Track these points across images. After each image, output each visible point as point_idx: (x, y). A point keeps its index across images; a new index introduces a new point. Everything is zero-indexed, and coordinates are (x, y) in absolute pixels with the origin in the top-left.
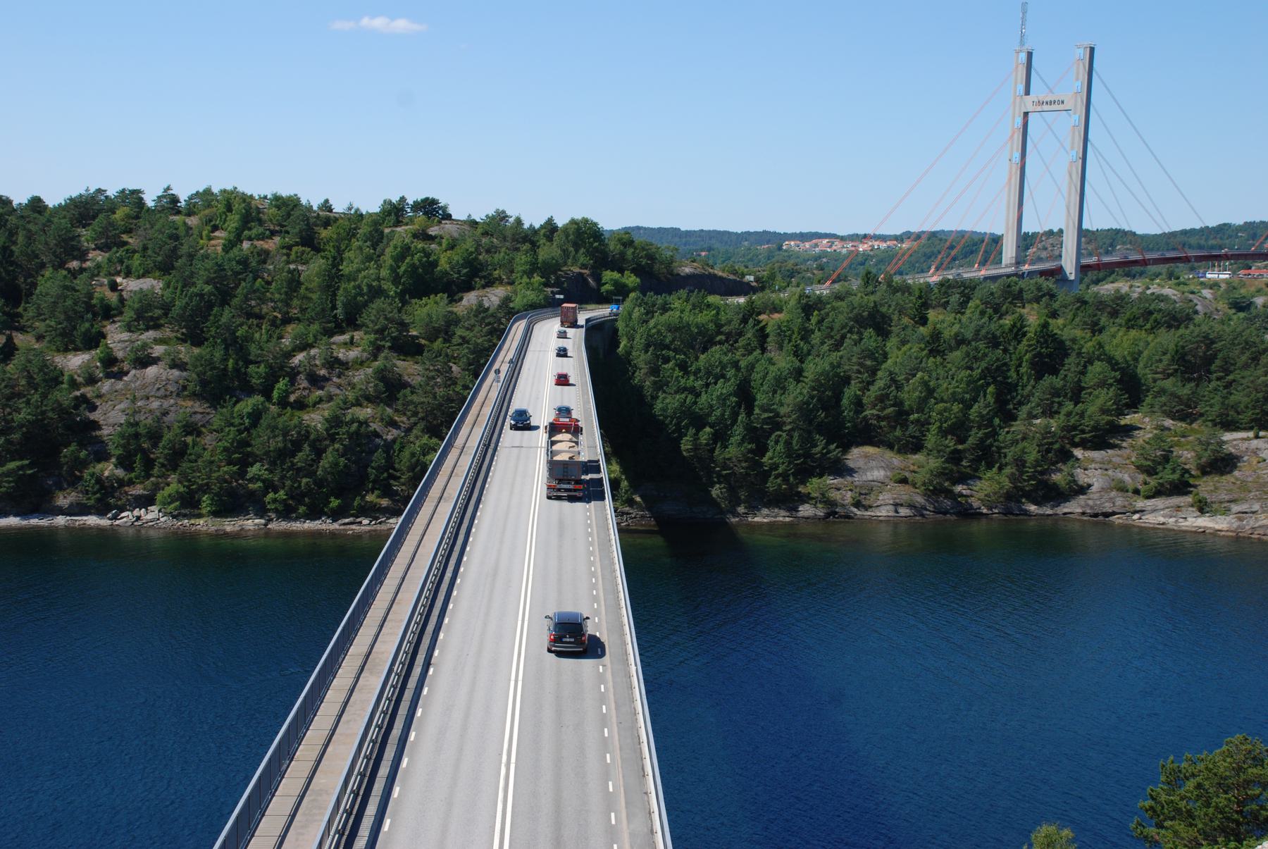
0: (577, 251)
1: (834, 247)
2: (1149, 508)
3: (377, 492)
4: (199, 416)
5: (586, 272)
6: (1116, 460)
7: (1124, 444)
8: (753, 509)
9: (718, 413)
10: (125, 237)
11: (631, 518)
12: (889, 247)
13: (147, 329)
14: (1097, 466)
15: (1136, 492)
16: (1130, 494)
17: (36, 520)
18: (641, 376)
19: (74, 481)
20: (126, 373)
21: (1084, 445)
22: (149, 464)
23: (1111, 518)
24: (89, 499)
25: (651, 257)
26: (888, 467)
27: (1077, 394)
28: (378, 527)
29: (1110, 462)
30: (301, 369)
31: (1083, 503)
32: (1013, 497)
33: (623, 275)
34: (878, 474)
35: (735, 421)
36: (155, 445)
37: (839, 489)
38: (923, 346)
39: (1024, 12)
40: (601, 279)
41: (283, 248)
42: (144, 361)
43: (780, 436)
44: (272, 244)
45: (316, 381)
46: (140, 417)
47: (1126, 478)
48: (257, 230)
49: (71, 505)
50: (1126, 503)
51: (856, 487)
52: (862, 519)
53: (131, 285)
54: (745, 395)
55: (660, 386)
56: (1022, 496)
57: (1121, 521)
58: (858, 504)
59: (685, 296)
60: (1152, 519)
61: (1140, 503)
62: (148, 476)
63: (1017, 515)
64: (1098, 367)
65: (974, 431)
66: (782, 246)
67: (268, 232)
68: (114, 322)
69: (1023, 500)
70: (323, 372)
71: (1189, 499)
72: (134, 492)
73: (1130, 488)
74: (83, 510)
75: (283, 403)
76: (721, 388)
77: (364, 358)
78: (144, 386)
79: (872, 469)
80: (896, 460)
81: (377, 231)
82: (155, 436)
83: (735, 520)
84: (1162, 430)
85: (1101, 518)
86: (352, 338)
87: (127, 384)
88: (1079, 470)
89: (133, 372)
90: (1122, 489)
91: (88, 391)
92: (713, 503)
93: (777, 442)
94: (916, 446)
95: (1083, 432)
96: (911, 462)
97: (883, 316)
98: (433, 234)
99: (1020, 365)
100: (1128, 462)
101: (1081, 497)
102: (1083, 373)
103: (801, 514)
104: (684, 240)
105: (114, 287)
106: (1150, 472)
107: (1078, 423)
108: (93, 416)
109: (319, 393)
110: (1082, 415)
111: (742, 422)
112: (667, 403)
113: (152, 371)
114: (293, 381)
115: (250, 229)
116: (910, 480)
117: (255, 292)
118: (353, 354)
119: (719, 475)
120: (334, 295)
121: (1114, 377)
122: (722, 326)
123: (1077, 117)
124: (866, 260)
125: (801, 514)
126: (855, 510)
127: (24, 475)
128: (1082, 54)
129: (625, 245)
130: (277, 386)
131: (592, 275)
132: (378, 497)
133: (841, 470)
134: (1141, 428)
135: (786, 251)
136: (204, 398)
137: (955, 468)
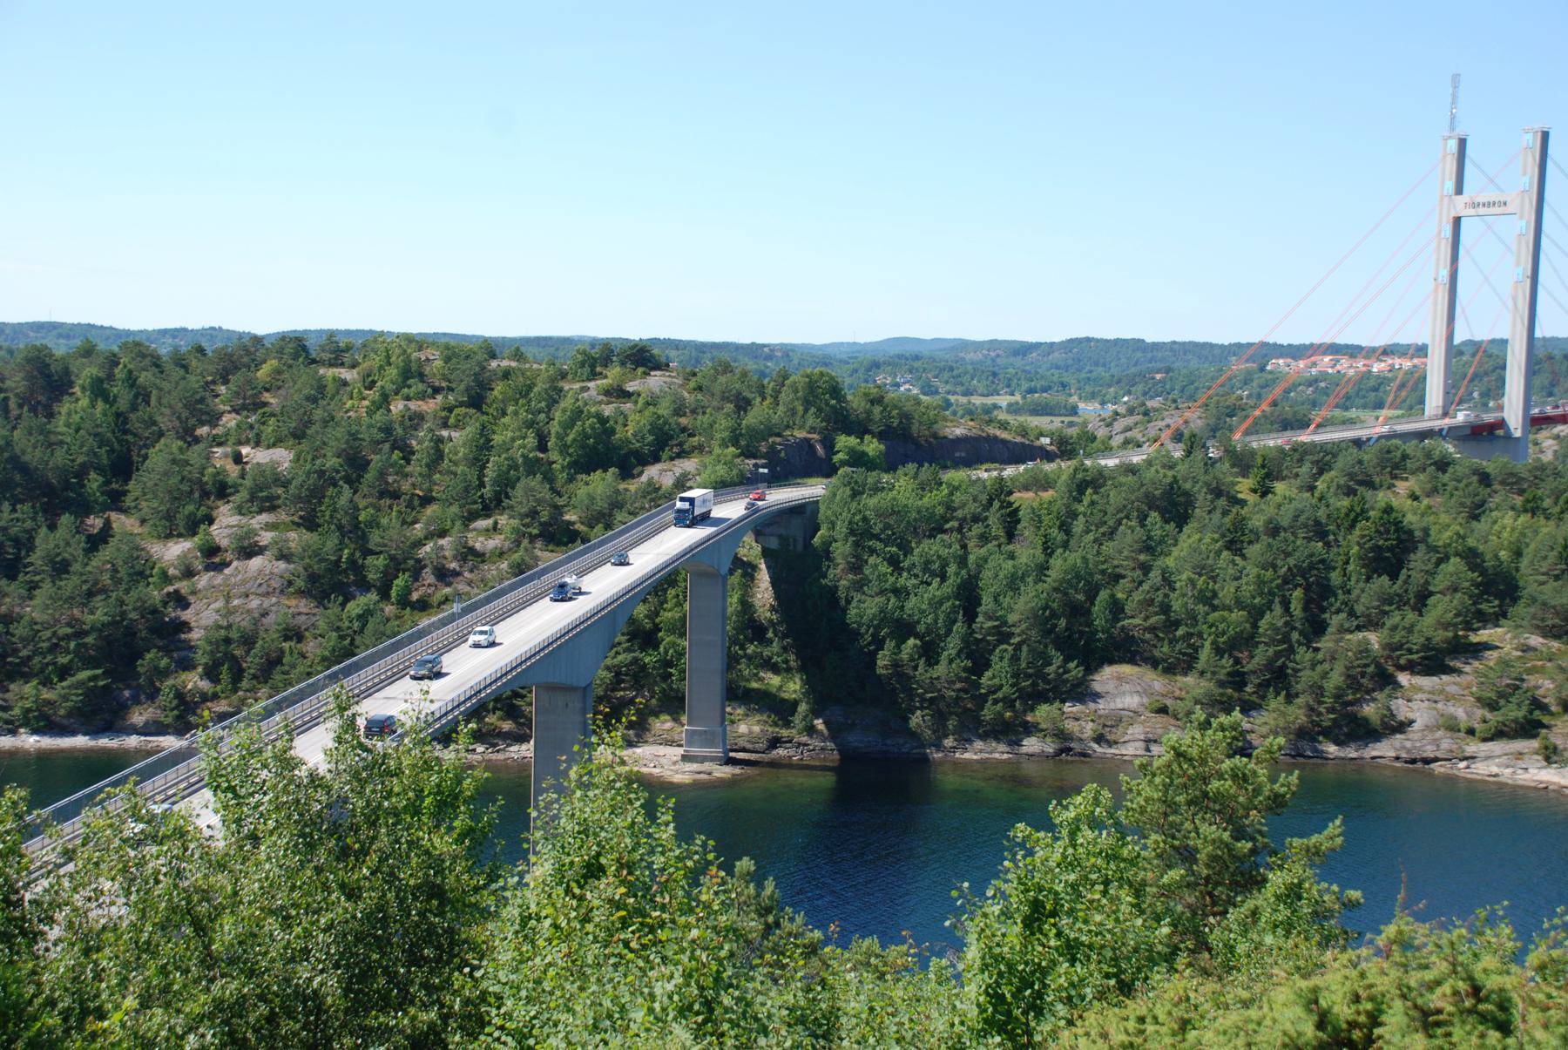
0: (806, 410)
1: (1338, 367)
2: (1483, 754)
3: (498, 713)
4: (304, 618)
5: (815, 436)
6: (1453, 689)
7: (1467, 669)
8: (964, 741)
9: (930, 620)
10: (267, 397)
11: (809, 751)
12: (1415, 366)
13: (260, 512)
14: (1425, 696)
15: (1471, 732)
16: (1462, 735)
17: (106, 740)
18: (838, 574)
19: (153, 695)
20: (228, 565)
21: (1410, 668)
22: (237, 674)
23: (1432, 766)
24: (166, 716)
25: (906, 417)
26: (1147, 692)
27: (1422, 599)
28: (494, 756)
29: (1442, 691)
30: (428, 562)
31: (1397, 744)
32: (1305, 737)
33: (862, 441)
34: (1131, 701)
35: (949, 632)
36: (248, 652)
37: (1077, 719)
38: (1216, 536)
39: (1455, 87)
40: (833, 446)
41: (444, 409)
42: (249, 551)
43: (1006, 650)
44: (430, 406)
45: (443, 575)
46: (237, 618)
47: (1460, 713)
48: (417, 387)
49: (147, 723)
50: (1455, 746)
51: (1100, 717)
52: (1102, 758)
53: (257, 456)
54: (968, 597)
55: (859, 586)
56: (1319, 733)
57: (1442, 770)
58: (1099, 739)
59: (912, 473)
60: (1481, 769)
61: (1473, 747)
62: (235, 690)
63: (1310, 757)
64: (1455, 564)
65: (1261, 647)
66: (1266, 364)
67: (430, 390)
68: (228, 502)
69: (1321, 738)
70: (453, 565)
71: (1534, 744)
72: (217, 709)
73: (1463, 726)
74: (158, 729)
75: (404, 602)
76: (935, 589)
77: (505, 549)
78: (244, 582)
79: (1124, 693)
80: (1158, 682)
81: (555, 389)
82: (248, 641)
83: (938, 755)
84: (1524, 651)
85: (1419, 765)
86: (496, 523)
87: (227, 578)
88: (1400, 701)
89: (235, 564)
90: (1452, 727)
91: (183, 586)
92: (913, 735)
93: (1001, 658)
94: (1183, 664)
95: (1410, 651)
96: (1179, 685)
97: (1187, 494)
98: (630, 389)
99: (1347, 562)
100: (1466, 692)
101: (1398, 736)
102: (1433, 574)
103: (1024, 750)
104: (1149, 355)
105: (238, 458)
106: (1492, 706)
107: (1404, 641)
108: (187, 615)
109: (447, 590)
110: (1410, 630)
111: (957, 632)
112: (864, 609)
113: (256, 562)
114: (416, 575)
115: (409, 387)
116: (1171, 709)
117: (392, 466)
118: (493, 543)
119: (923, 700)
120: (483, 467)
121: (1472, 580)
122: (955, 510)
123: (1525, 224)
124: (1380, 385)
125: (1024, 750)
126: (1095, 746)
127: (95, 686)
128: (1532, 141)
129: (872, 402)
130: (396, 582)
131: (822, 442)
132: (501, 719)
133: (1082, 693)
134: (1497, 647)
135: (1271, 372)
136: (313, 596)
137: (1236, 695)
